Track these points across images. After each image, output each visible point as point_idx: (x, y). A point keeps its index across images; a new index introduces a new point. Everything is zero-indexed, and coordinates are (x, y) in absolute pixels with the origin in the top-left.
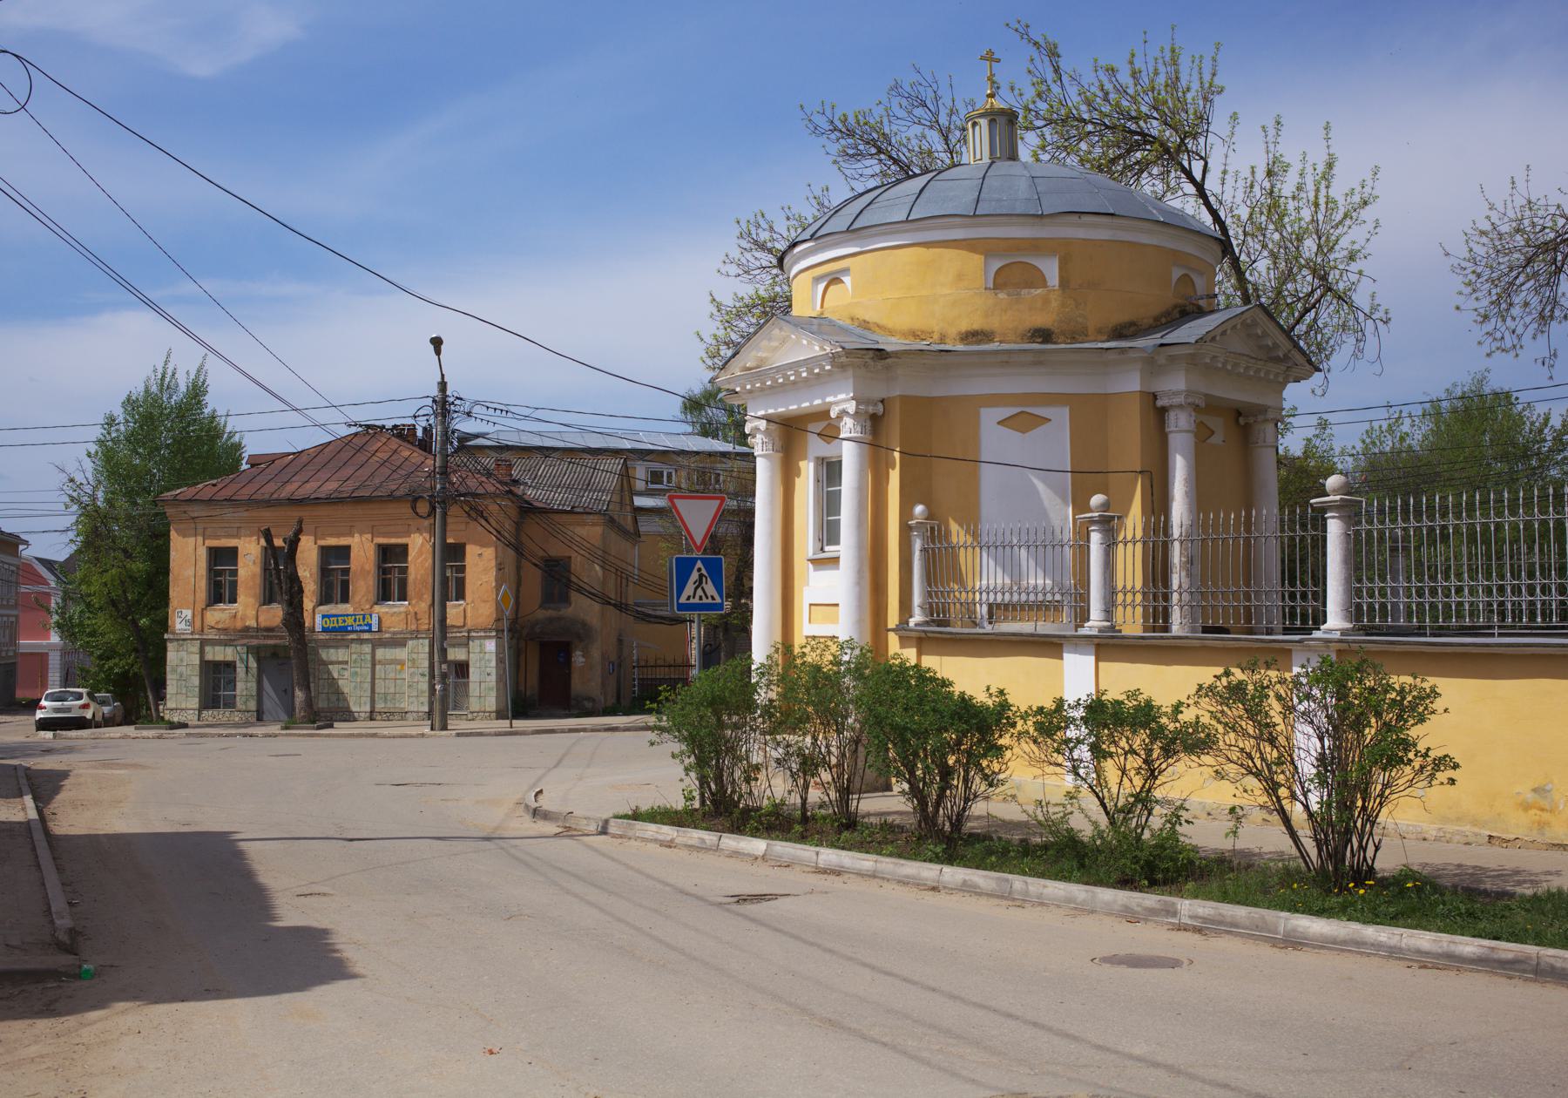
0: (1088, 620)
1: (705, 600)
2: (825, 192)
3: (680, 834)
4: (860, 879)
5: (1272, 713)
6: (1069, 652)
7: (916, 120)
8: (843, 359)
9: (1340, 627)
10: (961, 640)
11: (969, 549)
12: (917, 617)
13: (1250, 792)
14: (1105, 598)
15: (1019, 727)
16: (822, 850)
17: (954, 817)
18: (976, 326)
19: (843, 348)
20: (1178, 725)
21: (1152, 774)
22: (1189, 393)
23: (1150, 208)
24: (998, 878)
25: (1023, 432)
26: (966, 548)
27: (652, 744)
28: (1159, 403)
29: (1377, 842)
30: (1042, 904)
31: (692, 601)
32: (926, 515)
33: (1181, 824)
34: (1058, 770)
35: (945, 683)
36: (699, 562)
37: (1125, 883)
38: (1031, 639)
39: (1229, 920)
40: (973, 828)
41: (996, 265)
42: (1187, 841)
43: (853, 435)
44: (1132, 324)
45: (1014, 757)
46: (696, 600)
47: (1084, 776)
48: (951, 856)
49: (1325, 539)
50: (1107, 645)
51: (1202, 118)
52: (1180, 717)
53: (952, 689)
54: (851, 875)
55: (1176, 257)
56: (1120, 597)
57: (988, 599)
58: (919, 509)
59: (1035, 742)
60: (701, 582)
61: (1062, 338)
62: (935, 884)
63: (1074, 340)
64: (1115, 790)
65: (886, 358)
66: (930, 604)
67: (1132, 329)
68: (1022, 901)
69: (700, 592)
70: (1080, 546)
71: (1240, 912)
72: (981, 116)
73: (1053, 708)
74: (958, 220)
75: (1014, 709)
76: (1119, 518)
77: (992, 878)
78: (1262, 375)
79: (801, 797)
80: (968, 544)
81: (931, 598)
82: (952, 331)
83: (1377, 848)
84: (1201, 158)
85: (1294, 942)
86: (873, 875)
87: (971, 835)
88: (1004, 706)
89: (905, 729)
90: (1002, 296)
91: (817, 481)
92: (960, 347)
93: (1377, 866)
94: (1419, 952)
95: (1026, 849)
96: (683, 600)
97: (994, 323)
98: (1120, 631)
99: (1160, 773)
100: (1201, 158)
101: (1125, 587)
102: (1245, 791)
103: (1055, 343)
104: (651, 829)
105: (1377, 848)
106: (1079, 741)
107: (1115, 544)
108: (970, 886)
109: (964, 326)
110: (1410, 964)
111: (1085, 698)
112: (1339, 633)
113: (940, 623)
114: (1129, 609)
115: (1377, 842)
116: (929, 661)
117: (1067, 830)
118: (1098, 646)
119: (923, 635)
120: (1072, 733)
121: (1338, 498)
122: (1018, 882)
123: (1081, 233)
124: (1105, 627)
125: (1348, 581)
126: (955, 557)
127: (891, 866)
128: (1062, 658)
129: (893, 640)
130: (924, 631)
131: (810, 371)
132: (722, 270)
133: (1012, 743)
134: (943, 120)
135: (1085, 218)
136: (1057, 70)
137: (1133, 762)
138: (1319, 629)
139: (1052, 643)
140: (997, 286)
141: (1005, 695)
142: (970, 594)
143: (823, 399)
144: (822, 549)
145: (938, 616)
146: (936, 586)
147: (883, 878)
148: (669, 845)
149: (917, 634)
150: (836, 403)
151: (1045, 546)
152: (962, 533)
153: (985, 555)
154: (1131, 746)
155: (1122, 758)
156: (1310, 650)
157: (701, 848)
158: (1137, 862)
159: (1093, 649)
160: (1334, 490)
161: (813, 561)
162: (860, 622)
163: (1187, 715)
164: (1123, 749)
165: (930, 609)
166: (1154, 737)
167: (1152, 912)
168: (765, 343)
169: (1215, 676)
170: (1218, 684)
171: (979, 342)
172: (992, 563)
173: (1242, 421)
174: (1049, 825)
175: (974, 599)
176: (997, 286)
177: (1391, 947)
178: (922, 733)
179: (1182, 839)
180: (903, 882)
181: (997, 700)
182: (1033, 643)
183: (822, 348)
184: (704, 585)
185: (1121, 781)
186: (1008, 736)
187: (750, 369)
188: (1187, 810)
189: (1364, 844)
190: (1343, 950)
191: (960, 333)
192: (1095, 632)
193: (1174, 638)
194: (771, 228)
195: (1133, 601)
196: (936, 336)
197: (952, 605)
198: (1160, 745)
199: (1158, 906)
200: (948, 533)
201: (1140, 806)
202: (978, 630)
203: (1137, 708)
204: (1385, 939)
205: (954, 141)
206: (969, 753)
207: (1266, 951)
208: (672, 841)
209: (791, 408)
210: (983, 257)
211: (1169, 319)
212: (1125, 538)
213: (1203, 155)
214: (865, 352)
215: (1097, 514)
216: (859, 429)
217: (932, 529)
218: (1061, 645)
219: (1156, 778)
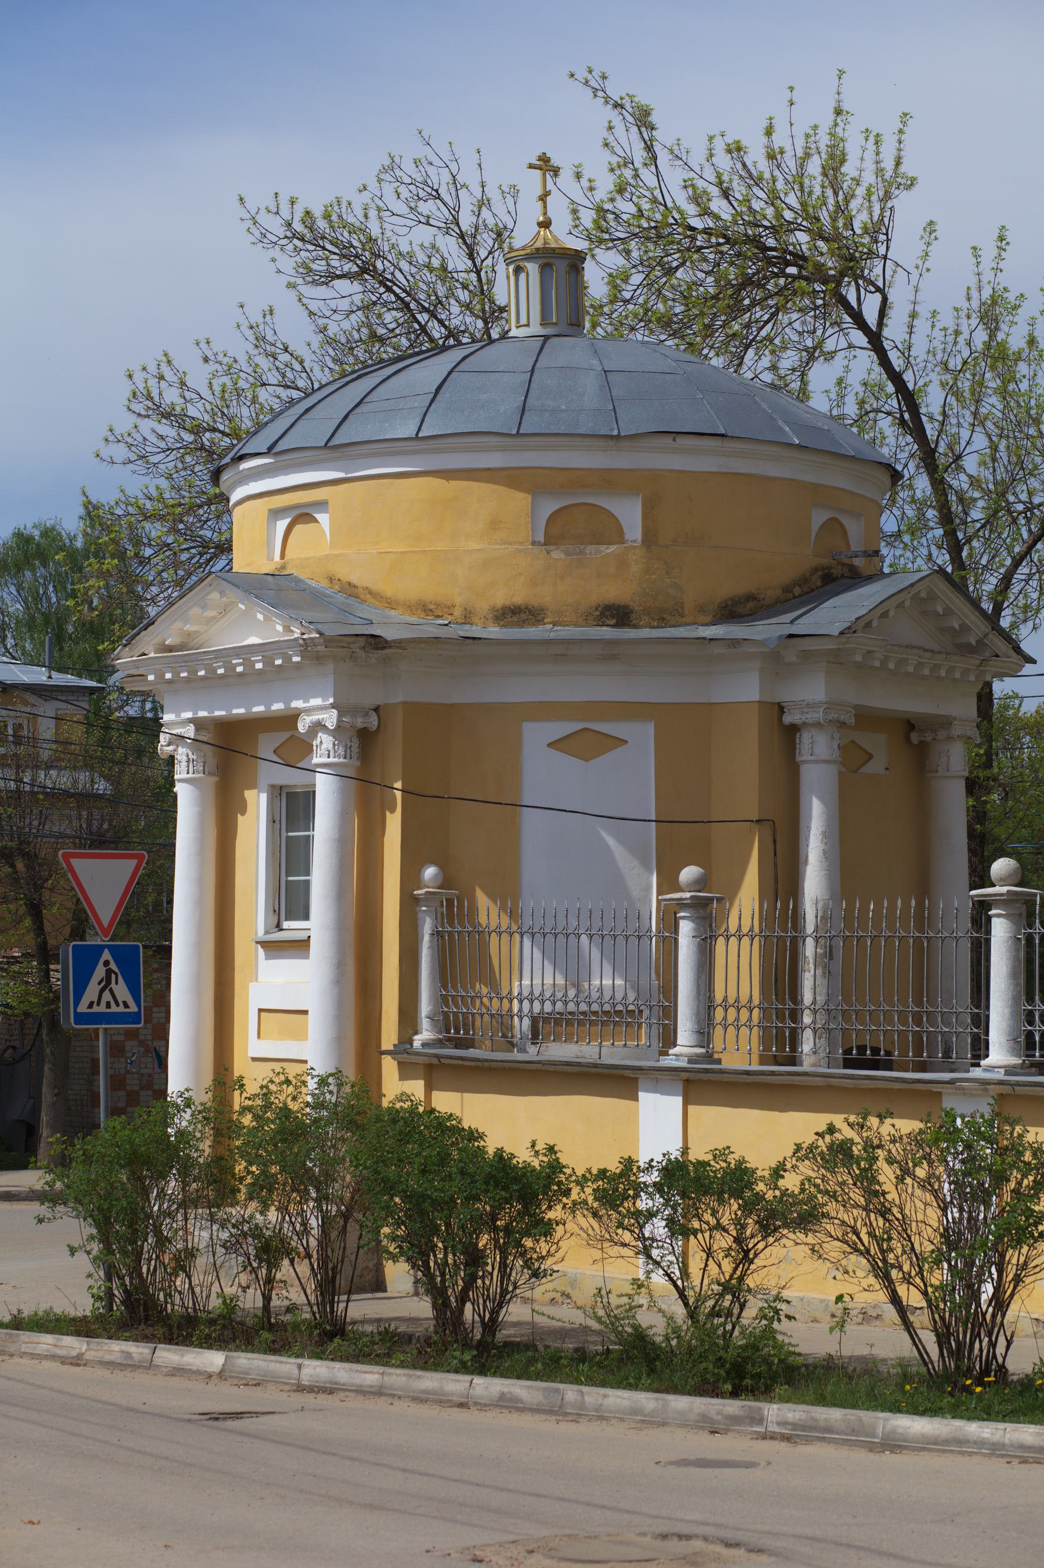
0: (675, 1045)
1: (114, 1009)
2: (268, 317)
3: (92, 1346)
4: (361, 1398)
5: (882, 1178)
6: (647, 1091)
7: (423, 220)
8: (321, 648)
9: (1005, 1063)
10: (490, 1069)
11: (505, 937)
12: (425, 1034)
13: (851, 1274)
14: (698, 1014)
15: (574, 1195)
16: (306, 1362)
17: (487, 1316)
18: (518, 600)
19: (321, 634)
20: (777, 1193)
21: (745, 1257)
22: (830, 705)
23: (780, 423)
24: (546, 1389)
25: (586, 760)
26: (500, 934)
27: (40, 1221)
28: (787, 719)
29: (1009, 1334)
30: (601, 1418)
31: (96, 1009)
32: (439, 882)
33: (779, 1320)
34: (626, 1252)
35: (474, 1136)
36: (106, 950)
37: (706, 1388)
38: (594, 1070)
39: (822, 1424)
40: (509, 1336)
41: (550, 506)
42: (787, 1340)
43: (332, 760)
44: (750, 597)
45: (568, 1235)
46: (102, 1009)
47: (658, 1259)
48: (483, 1365)
49: (988, 941)
50: (700, 1081)
51: (878, 229)
52: (781, 1183)
53: (482, 1143)
54: (347, 1393)
55: (818, 493)
56: (719, 1013)
57: (531, 1010)
58: (430, 872)
59: (595, 1215)
60: (109, 982)
61: (645, 620)
62: (462, 1400)
63: (663, 622)
64: (697, 1282)
65: (384, 648)
66: (446, 1015)
67: (750, 605)
68: (579, 1414)
69: (107, 996)
70: (664, 938)
71: (835, 1415)
72: (529, 257)
73: (618, 1171)
74: (493, 440)
75: (568, 1171)
76: (720, 900)
77: (538, 1389)
78: (943, 673)
79: (263, 1295)
80: (504, 928)
81: (447, 1006)
82: (483, 606)
83: (1009, 1343)
84: (878, 290)
85: (893, 1444)
86: (378, 1392)
87: (506, 1344)
88: (555, 1167)
89: (423, 1197)
90: (557, 554)
91: (272, 821)
92: (494, 631)
93: (1011, 1365)
94: (1022, 1447)
95: (581, 1356)
96: (83, 1008)
97: (544, 595)
98: (719, 1061)
99: (756, 1255)
100: (878, 290)
101: (725, 999)
102: (846, 1272)
103: (635, 626)
104: (46, 1342)
105: (1009, 1343)
106: (651, 1215)
107: (713, 938)
108: (511, 1400)
109: (501, 598)
110: (1009, 1460)
111: (660, 1158)
112: (1002, 1071)
113: (459, 1044)
114: (731, 1030)
115: (1009, 1334)
116: (445, 1102)
117: (633, 1326)
118: (687, 1082)
119: (435, 1061)
120: (644, 1203)
121: (1004, 889)
122: (571, 1393)
123: (675, 462)
124: (697, 1055)
125: (1015, 1002)
126: (484, 946)
127: (404, 1379)
128: (636, 1099)
129: (389, 1067)
130: (436, 1056)
131: (268, 661)
132: (102, 454)
133: (565, 1217)
134: (466, 222)
135: (682, 441)
136: (649, 148)
137: (723, 1242)
138: (978, 1065)
139: (624, 1078)
140: (550, 540)
141: (556, 1153)
142: (505, 1001)
143: (287, 703)
144: (279, 927)
145: (457, 1032)
146: (456, 990)
147: (393, 1396)
148: (77, 1361)
149: (427, 1060)
150: (308, 711)
151: (615, 937)
152: (494, 911)
153: (527, 942)
154: (718, 1221)
155: (707, 1235)
156: (965, 1094)
157: (126, 1365)
158: (722, 1366)
159: (680, 1087)
160: (1001, 879)
161: (265, 944)
162: (339, 1040)
163: (791, 1182)
164: (708, 1223)
165: (444, 1022)
166: (748, 1208)
167: (735, 1420)
168: (196, 611)
169: (817, 1134)
170: (820, 1143)
171: (522, 623)
172: (538, 955)
173: (915, 738)
174: (613, 1321)
175: (510, 1009)
176: (550, 540)
177: (993, 1444)
178: (446, 1203)
179: (779, 1337)
180: (421, 1398)
181: (546, 1159)
182: (597, 1076)
183: (287, 629)
184: (113, 985)
185: (706, 1265)
186: (559, 1207)
187: (170, 649)
188: (788, 1302)
189: (994, 1339)
190: (944, 1451)
191: (493, 609)
192: (683, 1063)
193: (806, 1074)
194: (183, 384)
195: (737, 1019)
196: (458, 612)
197: (478, 1019)
198: (756, 1218)
199: (741, 1413)
200: (474, 909)
201: (729, 1297)
202: (516, 1055)
203: (728, 1172)
204: (988, 1435)
205: (483, 254)
206: (508, 1230)
207: (861, 1455)
208: (80, 1356)
209: (235, 711)
210: (530, 497)
211: (805, 589)
212: (727, 930)
213: (880, 284)
214: (355, 638)
215: (688, 895)
216: (341, 751)
217: (450, 902)
218: (636, 1080)
219: (752, 1262)
